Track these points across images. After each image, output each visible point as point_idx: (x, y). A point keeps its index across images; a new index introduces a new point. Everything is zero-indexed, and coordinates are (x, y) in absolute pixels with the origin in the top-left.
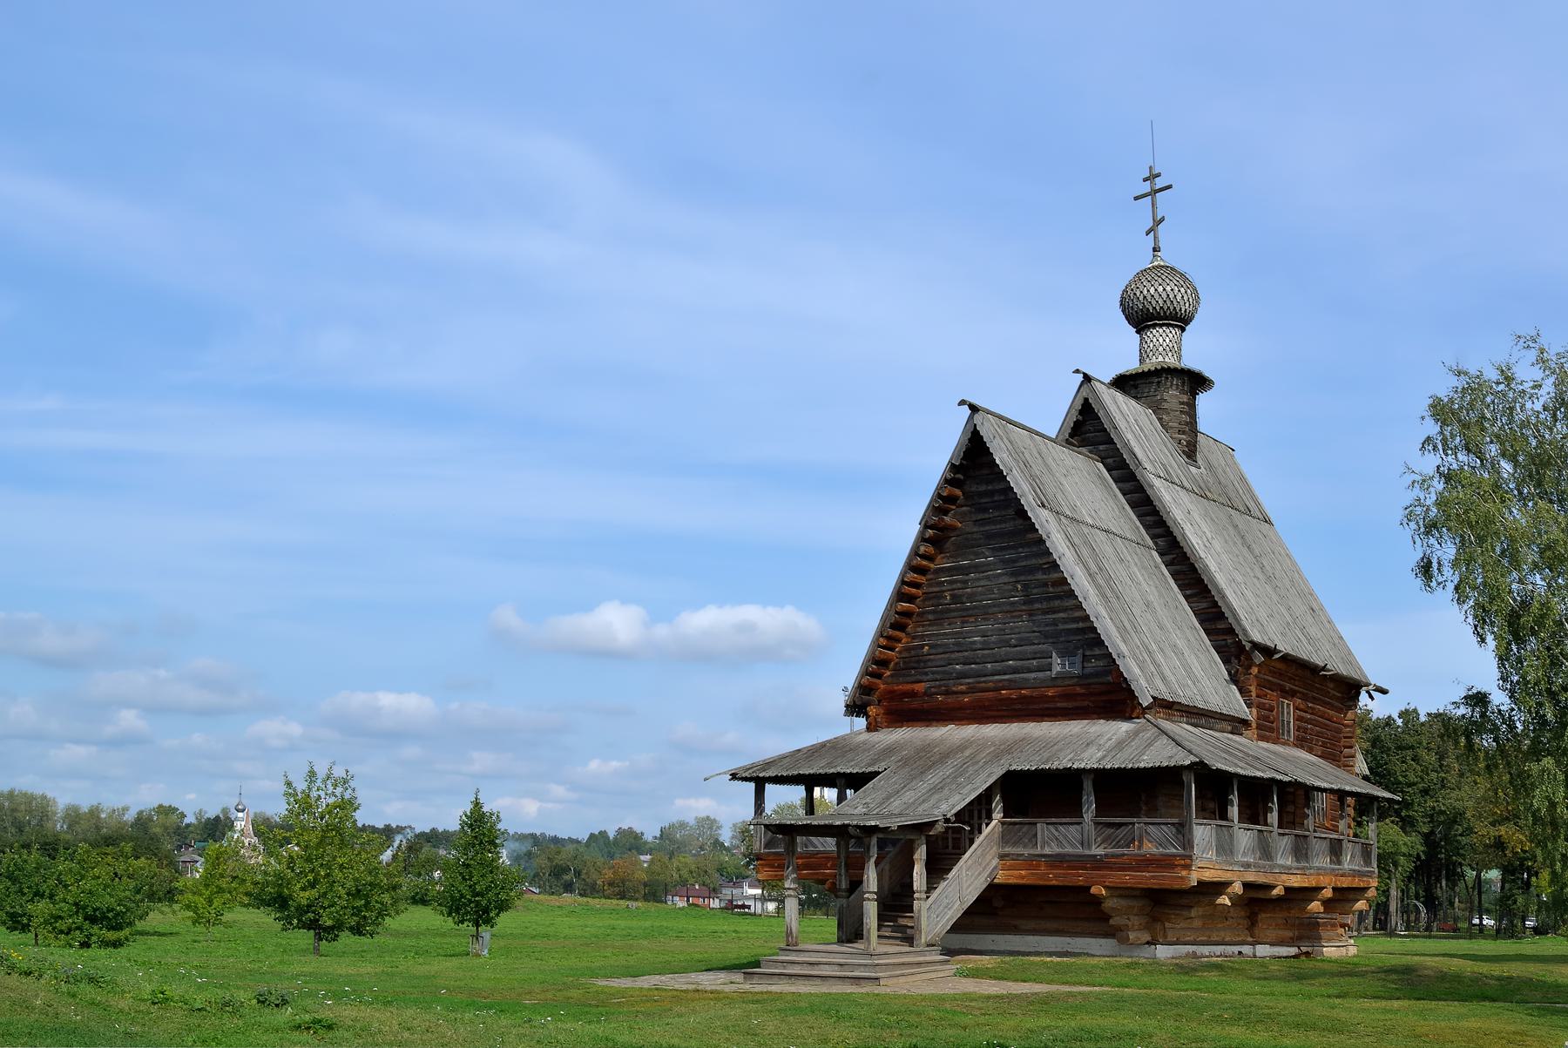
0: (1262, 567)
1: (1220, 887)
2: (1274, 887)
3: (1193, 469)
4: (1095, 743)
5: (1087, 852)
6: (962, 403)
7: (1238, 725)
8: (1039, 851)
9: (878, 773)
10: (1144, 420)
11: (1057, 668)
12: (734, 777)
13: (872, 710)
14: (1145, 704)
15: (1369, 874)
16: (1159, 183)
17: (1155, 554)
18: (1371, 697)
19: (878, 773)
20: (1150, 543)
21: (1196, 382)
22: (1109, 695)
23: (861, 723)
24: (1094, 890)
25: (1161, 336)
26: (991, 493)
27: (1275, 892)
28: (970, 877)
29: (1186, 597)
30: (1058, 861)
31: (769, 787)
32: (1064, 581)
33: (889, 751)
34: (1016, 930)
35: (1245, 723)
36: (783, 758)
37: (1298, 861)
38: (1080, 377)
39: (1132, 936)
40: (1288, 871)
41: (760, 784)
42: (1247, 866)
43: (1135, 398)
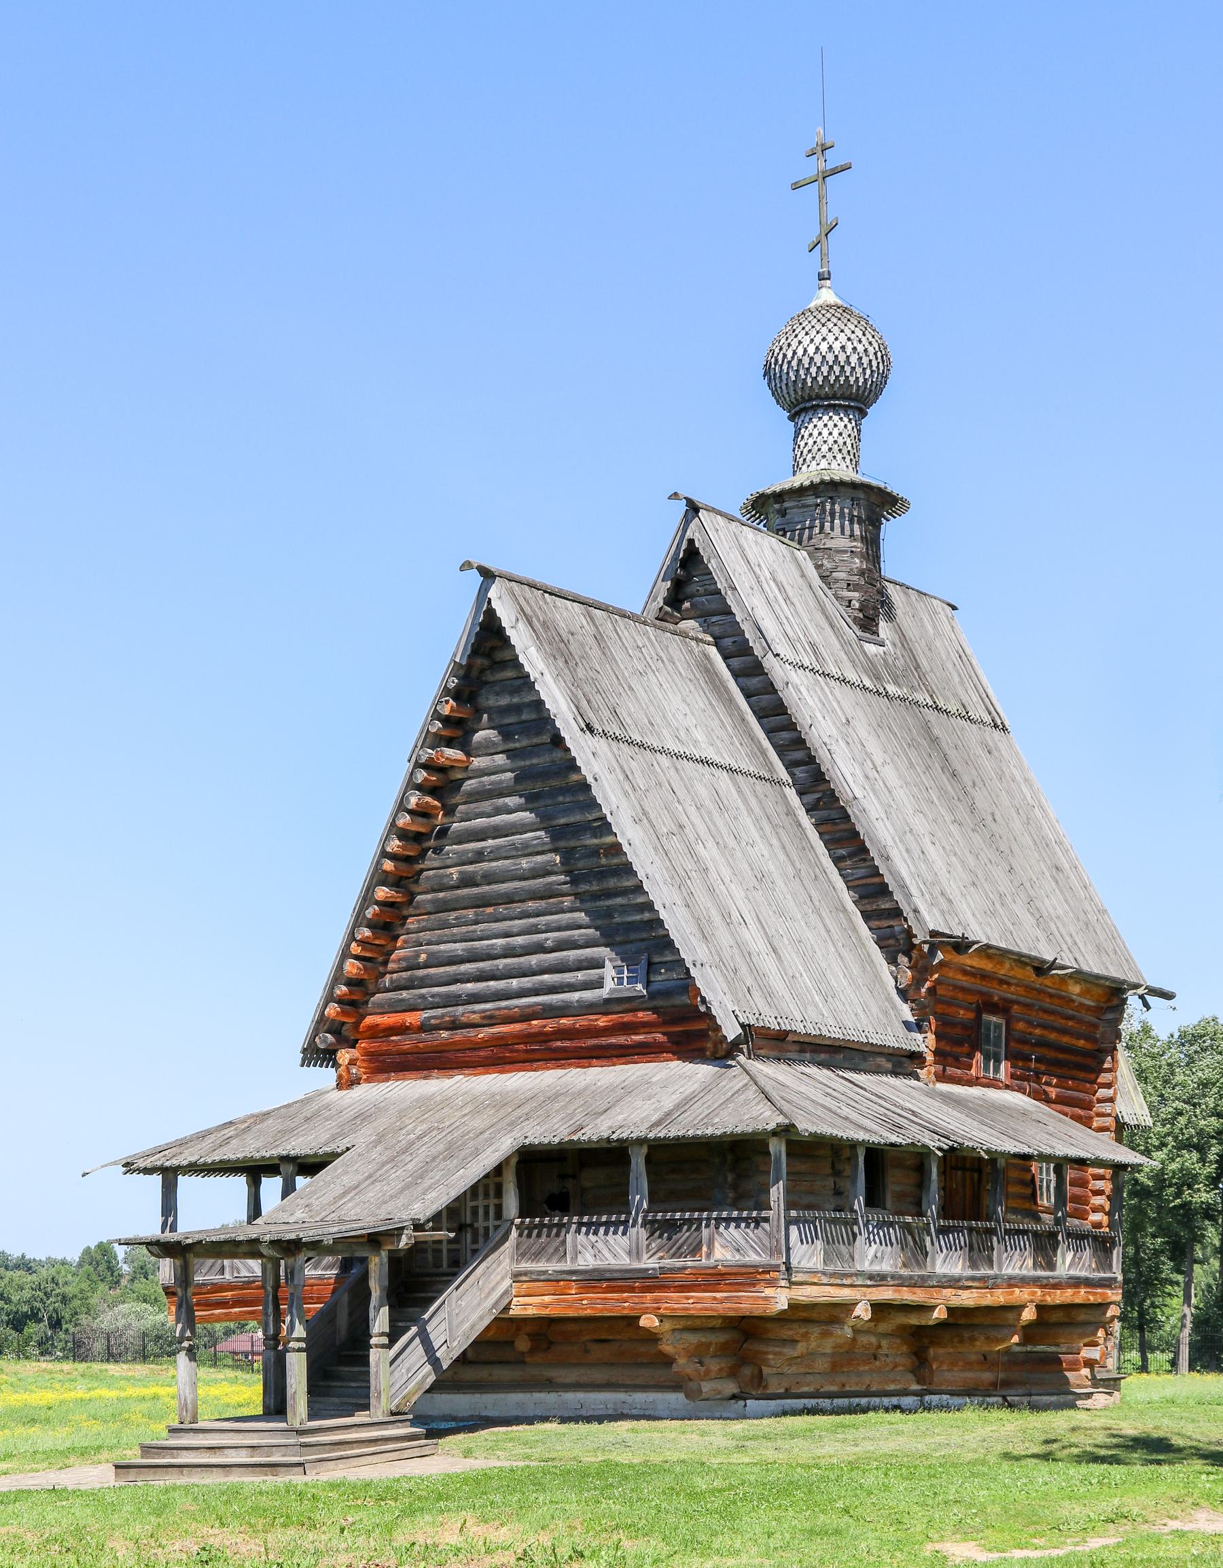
0: (972, 809)
1: (836, 1312)
2: (933, 1308)
3: (871, 649)
4: (649, 1098)
5: (637, 1265)
6: (466, 566)
7: (903, 1063)
8: (567, 1265)
9: (335, 1155)
10: (788, 575)
11: (609, 985)
12: (129, 1167)
13: (344, 1056)
14: (731, 1037)
15: (1107, 1283)
16: (834, 159)
17: (791, 793)
18: (1146, 1005)
19: (335, 1155)
20: (784, 774)
21: (875, 505)
22: (684, 1029)
23: (325, 1076)
24: (643, 1322)
25: (828, 428)
26: (517, 709)
27: (935, 1315)
28: (464, 1311)
29: (837, 861)
30: (595, 1280)
31: (185, 1183)
32: (617, 849)
33: (363, 1117)
34: (550, 1385)
35: (916, 1057)
36: (203, 1136)
37: (974, 1265)
38: (682, 506)
39: (706, 1387)
40: (954, 1283)
41: (170, 1175)
42: (879, 1279)
43: (781, 531)
